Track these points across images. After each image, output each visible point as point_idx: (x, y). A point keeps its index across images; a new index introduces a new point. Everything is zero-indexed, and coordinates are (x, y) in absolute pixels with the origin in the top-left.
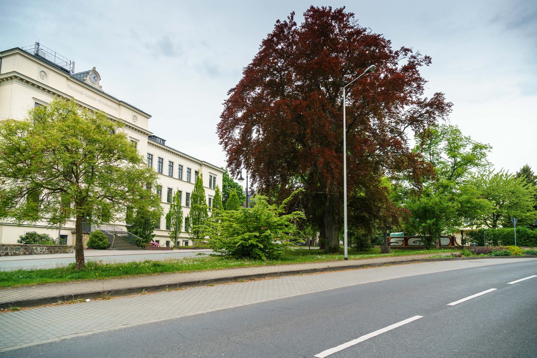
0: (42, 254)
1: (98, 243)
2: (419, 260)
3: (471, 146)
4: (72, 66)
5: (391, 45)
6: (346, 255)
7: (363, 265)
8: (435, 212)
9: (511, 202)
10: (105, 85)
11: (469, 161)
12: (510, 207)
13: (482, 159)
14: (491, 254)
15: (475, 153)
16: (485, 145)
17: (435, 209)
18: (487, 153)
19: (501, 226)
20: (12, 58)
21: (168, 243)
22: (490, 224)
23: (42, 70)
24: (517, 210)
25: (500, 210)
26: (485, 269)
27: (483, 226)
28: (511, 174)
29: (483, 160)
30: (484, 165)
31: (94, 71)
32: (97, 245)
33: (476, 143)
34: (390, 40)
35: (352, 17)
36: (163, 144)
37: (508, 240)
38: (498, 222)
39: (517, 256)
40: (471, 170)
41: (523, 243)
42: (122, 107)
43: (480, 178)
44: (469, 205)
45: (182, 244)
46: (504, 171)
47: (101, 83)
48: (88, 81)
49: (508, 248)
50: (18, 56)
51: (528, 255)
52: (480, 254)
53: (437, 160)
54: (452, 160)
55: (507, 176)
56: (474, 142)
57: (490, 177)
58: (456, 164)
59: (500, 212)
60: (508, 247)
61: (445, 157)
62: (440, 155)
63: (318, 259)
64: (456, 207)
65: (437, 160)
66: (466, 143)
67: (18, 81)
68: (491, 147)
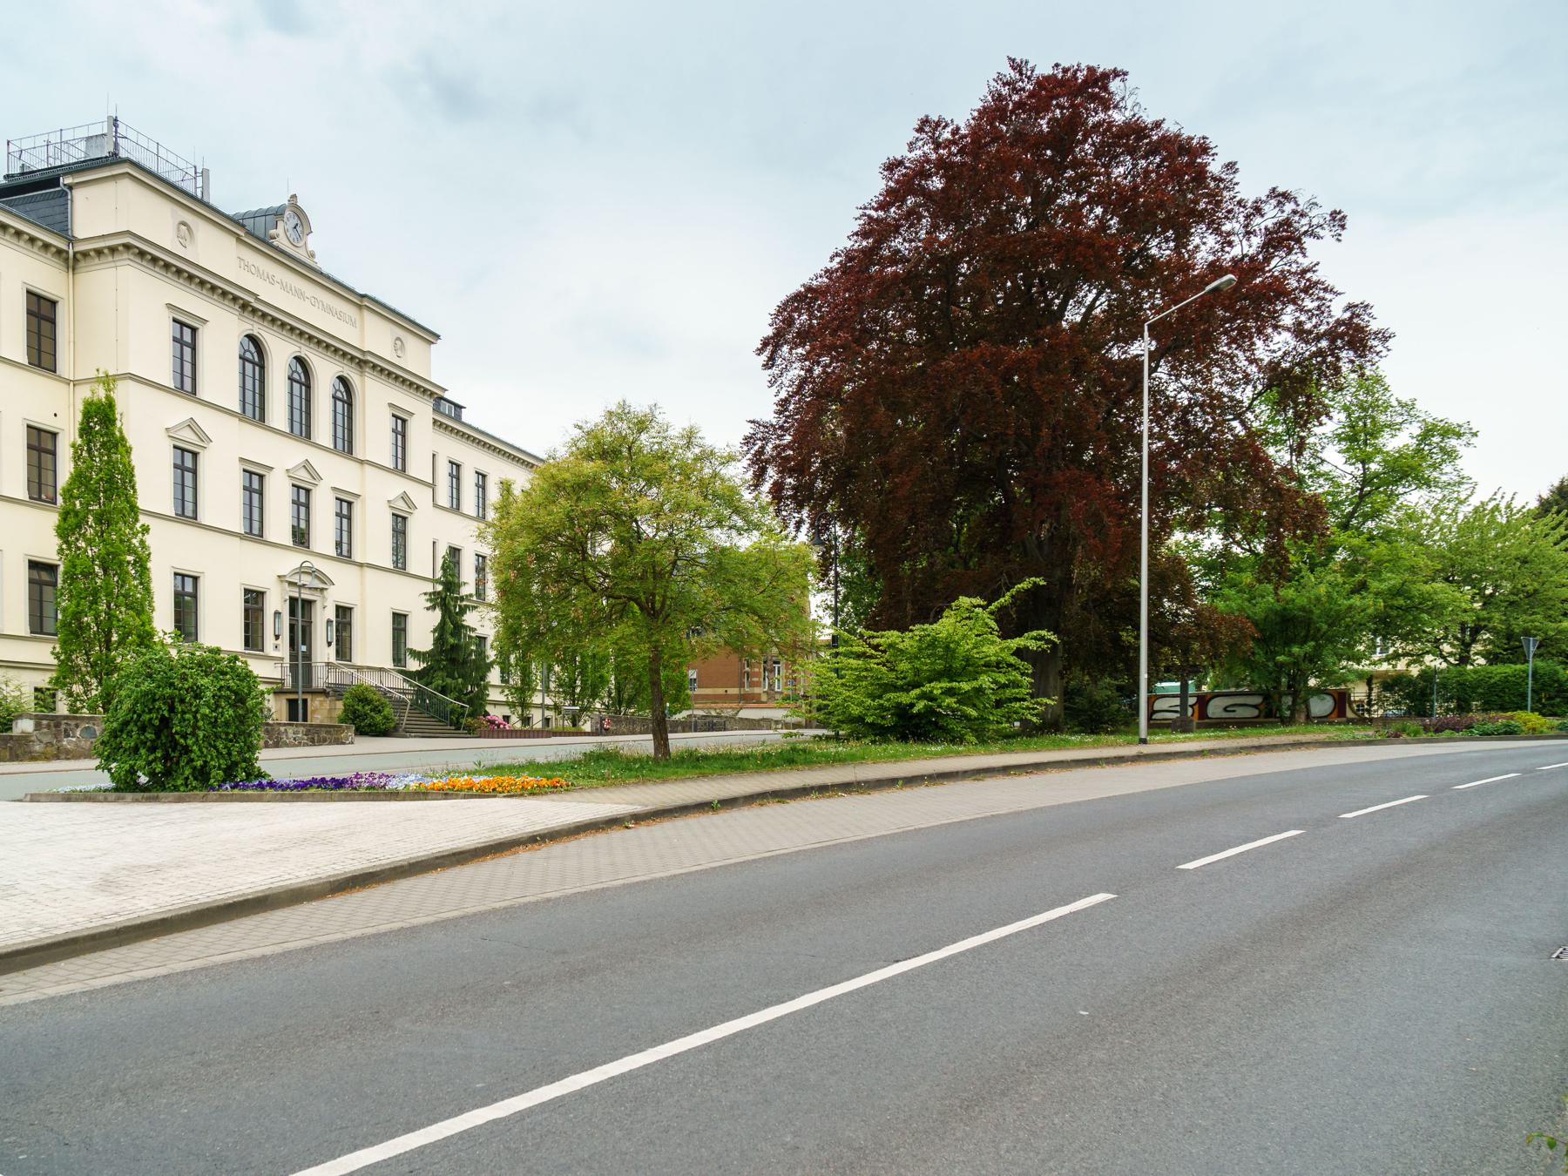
0: (297, 746)
1: (372, 717)
2: (1309, 743)
3: (1416, 429)
4: (199, 180)
5: (1237, 175)
6: (1143, 734)
7: (1202, 751)
8: (1315, 623)
9: (1518, 590)
10: (324, 249)
11: (1405, 470)
12: (1512, 603)
13: (1444, 465)
14: (1471, 732)
15: (1427, 448)
16: (1459, 426)
17: (1314, 617)
18: (1462, 450)
19: (1482, 661)
20: (109, 187)
21: (547, 721)
22: (1451, 654)
23: (181, 219)
24: (1534, 613)
25: (1484, 614)
26: (1476, 754)
27: (1428, 658)
28: (1524, 507)
29: (1447, 468)
30: (1449, 484)
31: (299, 213)
32: (370, 725)
33: (1430, 420)
34: (1235, 163)
35: (1118, 79)
36: (458, 419)
37: (1502, 697)
38: (1477, 647)
39: (1535, 734)
40: (1407, 497)
41: (1544, 706)
42: (366, 313)
43: (1428, 517)
44: (1401, 601)
45: (537, 723)
46: (1503, 497)
47: (312, 242)
48: (282, 242)
49: (1511, 718)
50: (126, 184)
51: (1564, 733)
52: (1442, 731)
53: (1311, 467)
54: (1357, 469)
55: (1512, 510)
56: (1423, 416)
57: (1461, 517)
58: (1366, 480)
59: (1484, 620)
60: (1509, 713)
61: (1334, 459)
62: (1319, 455)
63: (1068, 741)
64: (1370, 611)
65: (1311, 467)
66: (1399, 420)
67: (132, 257)
68: (1474, 431)
